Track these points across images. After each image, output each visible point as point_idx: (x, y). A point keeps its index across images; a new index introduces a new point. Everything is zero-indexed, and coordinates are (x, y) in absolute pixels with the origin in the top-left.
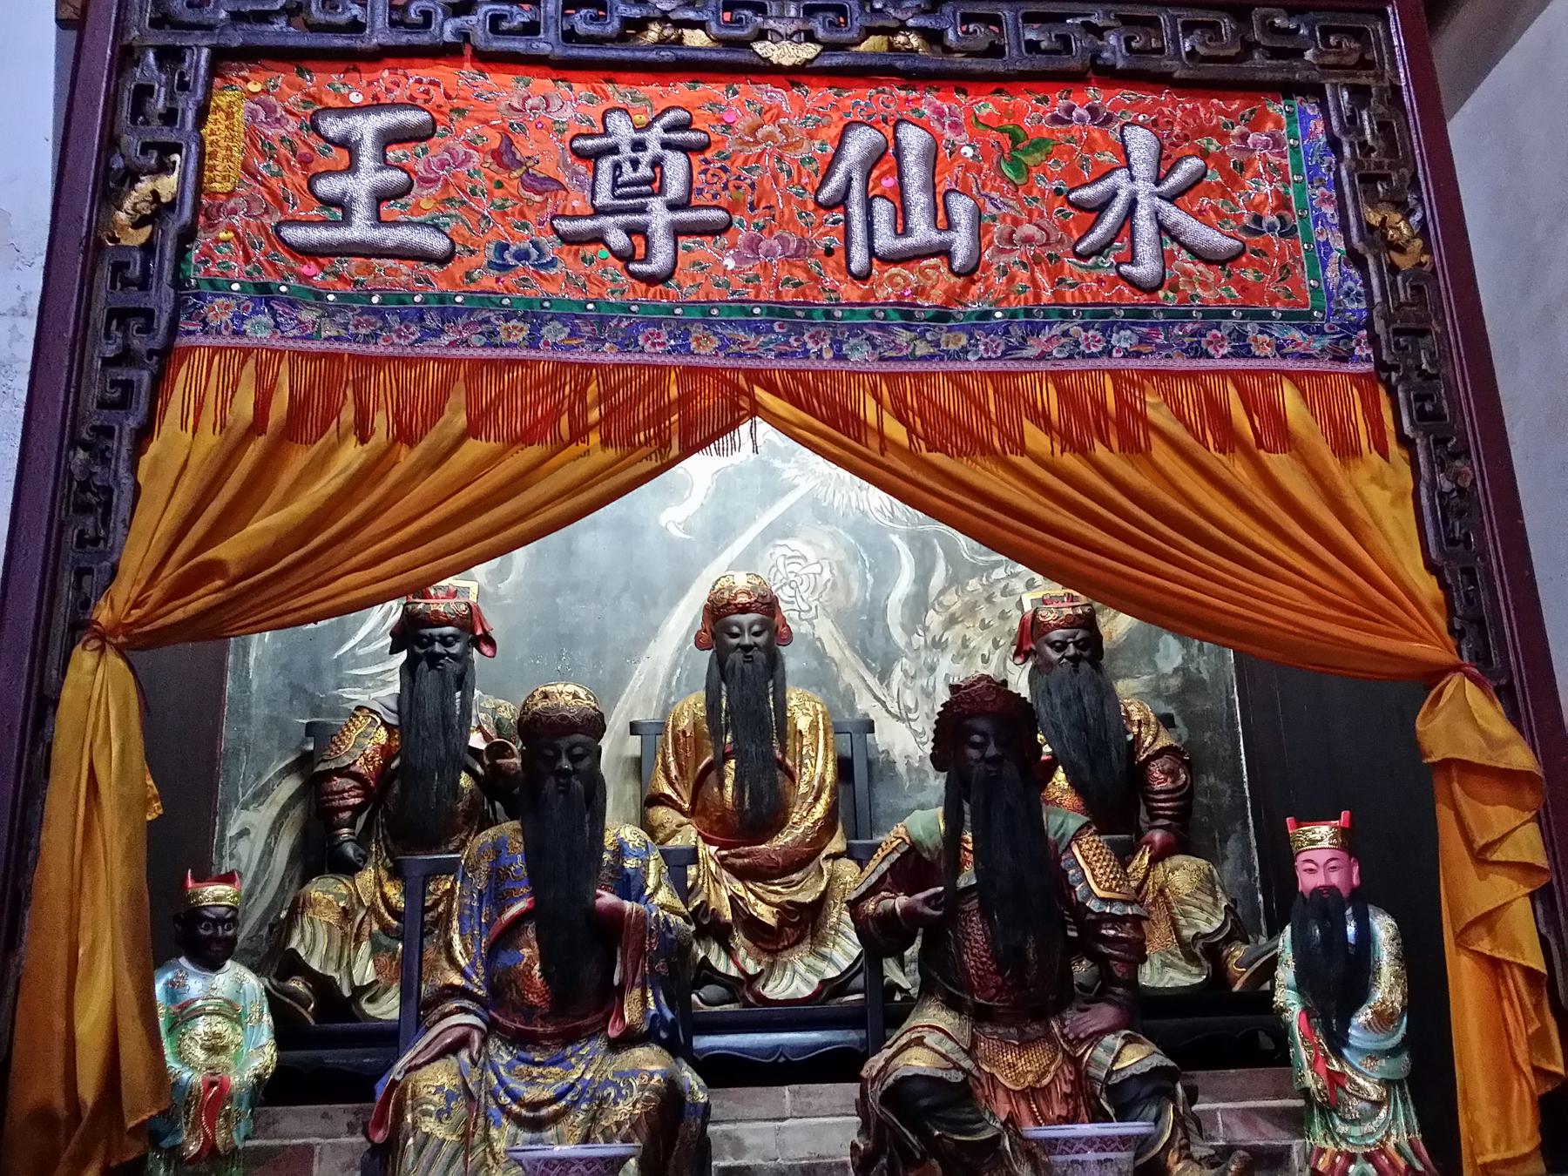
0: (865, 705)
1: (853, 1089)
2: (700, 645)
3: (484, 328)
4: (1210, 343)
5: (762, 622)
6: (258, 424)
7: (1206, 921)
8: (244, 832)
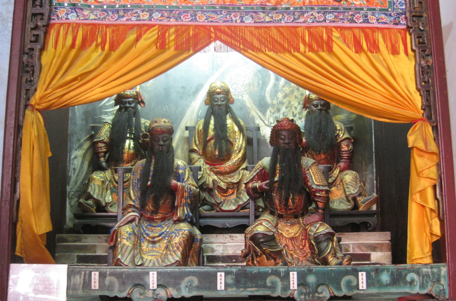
0: (258, 121)
1: (244, 235)
2: (206, 104)
3: (136, 15)
4: (356, 18)
5: (224, 98)
6: (73, 45)
7: (353, 191)
8: (76, 157)
